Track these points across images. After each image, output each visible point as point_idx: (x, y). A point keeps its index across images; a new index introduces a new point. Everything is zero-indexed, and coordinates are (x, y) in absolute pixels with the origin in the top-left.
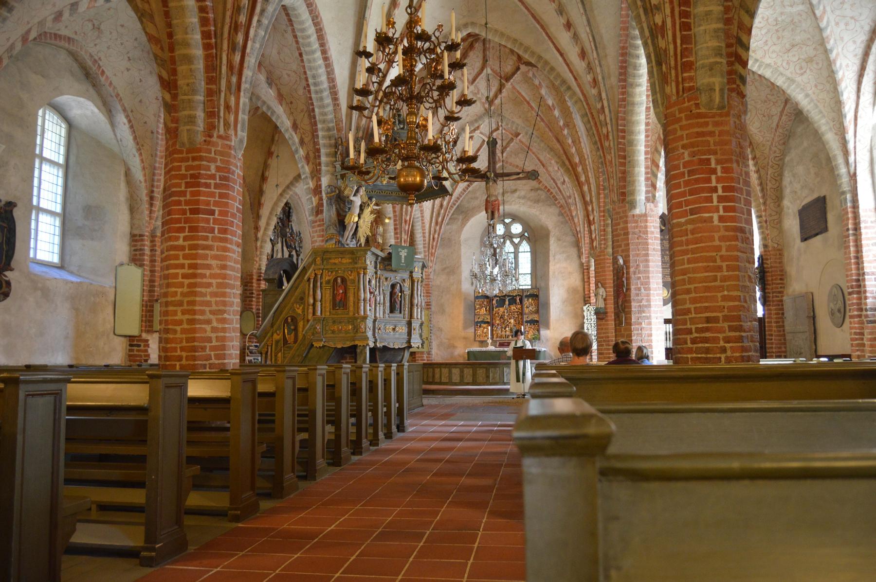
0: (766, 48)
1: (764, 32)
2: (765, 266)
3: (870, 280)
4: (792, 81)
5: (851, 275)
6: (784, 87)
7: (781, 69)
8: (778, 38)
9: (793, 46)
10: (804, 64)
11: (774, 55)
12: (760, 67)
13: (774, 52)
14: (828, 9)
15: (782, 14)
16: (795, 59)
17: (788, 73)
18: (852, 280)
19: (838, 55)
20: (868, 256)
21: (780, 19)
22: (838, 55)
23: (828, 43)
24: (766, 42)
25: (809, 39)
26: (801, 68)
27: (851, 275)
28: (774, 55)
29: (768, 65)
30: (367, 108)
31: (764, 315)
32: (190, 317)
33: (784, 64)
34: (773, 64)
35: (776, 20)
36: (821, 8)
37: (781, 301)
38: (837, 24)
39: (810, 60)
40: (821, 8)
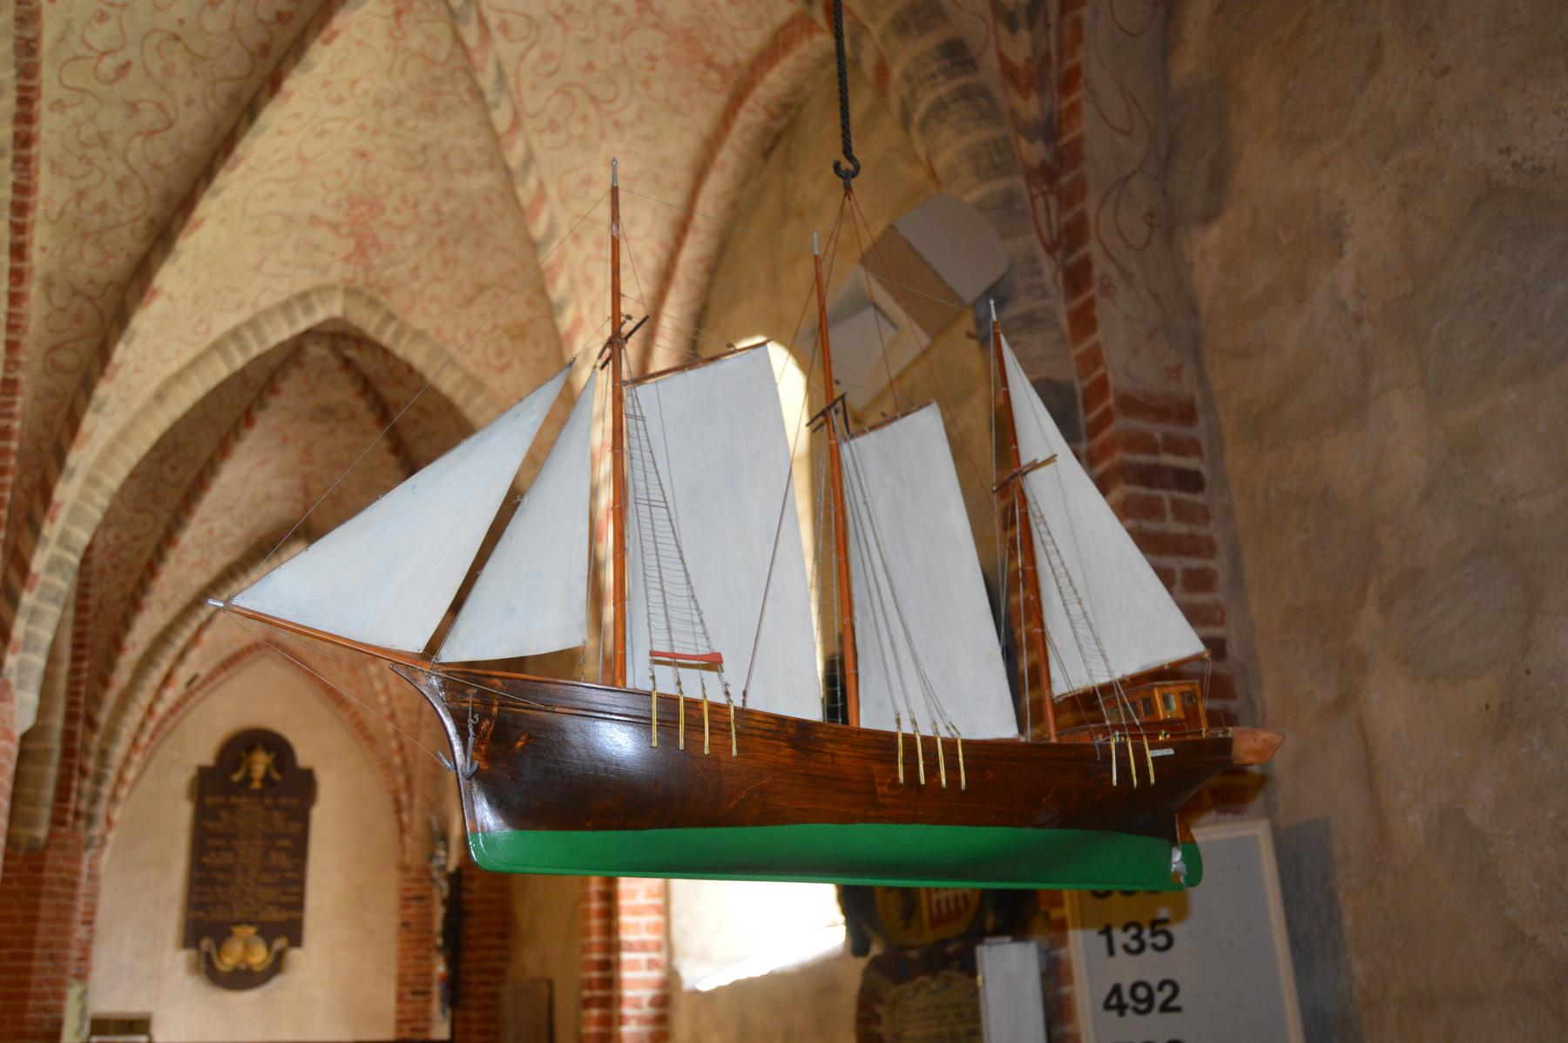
0: (416, 286)
1: (410, 238)
2: (466, 896)
3: (635, 965)
4: (478, 385)
5: (586, 949)
6: (459, 398)
7: (452, 350)
8: (446, 263)
9: (480, 289)
10: (506, 342)
11: (435, 309)
12: (398, 334)
13: (434, 299)
14: (552, 191)
15: (449, 193)
16: (486, 327)
17: (467, 362)
18: (589, 965)
19: (578, 322)
20: (633, 894)
21: (445, 208)
22: (578, 322)
23: (553, 282)
24: (415, 272)
25: (514, 273)
26: (500, 353)
27: (586, 949)
28: (435, 309)
29: (419, 335)
30: (1002, 58)
31: (453, 1031)
32: (1194, 563)
33: (461, 337)
34: (432, 332)
35: (437, 210)
36: (532, 182)
37: (495, 996)
38: (576, 238)
39: (518, 333)
40: (532, 182)
